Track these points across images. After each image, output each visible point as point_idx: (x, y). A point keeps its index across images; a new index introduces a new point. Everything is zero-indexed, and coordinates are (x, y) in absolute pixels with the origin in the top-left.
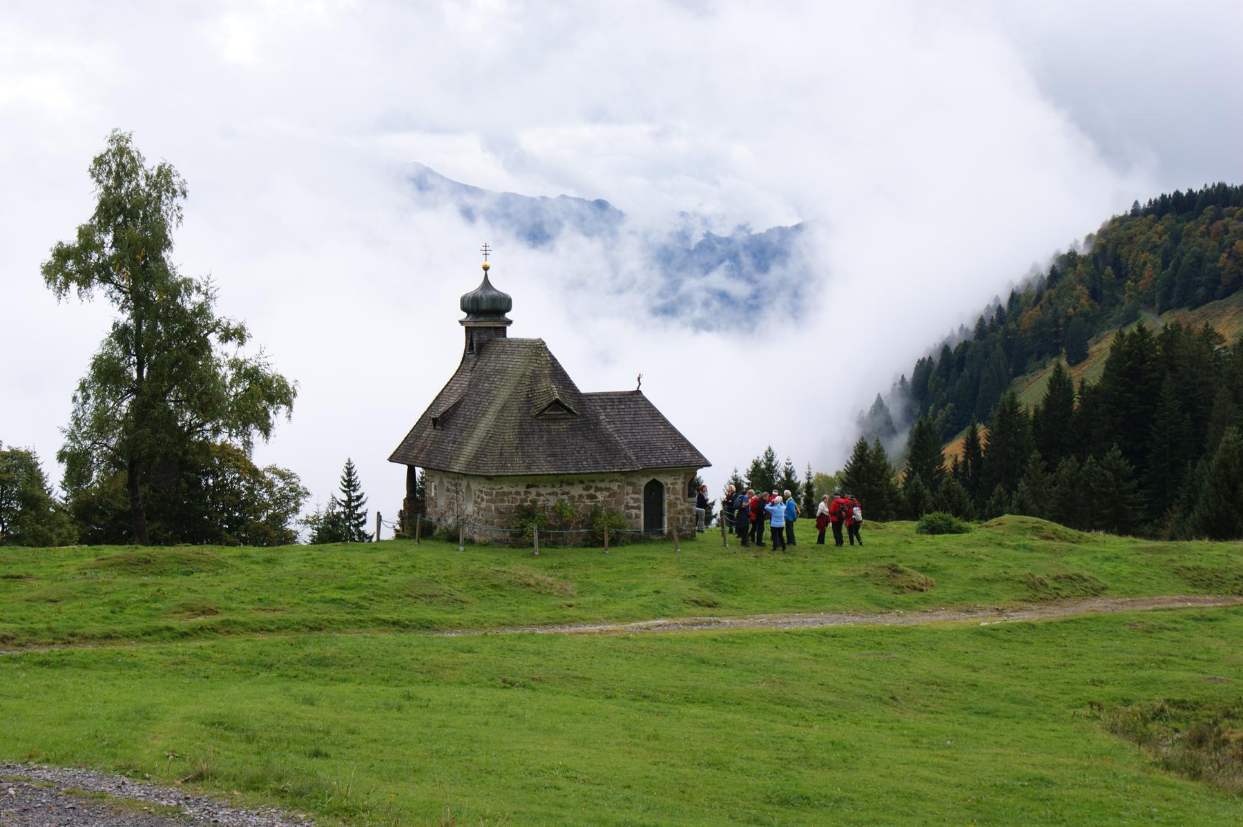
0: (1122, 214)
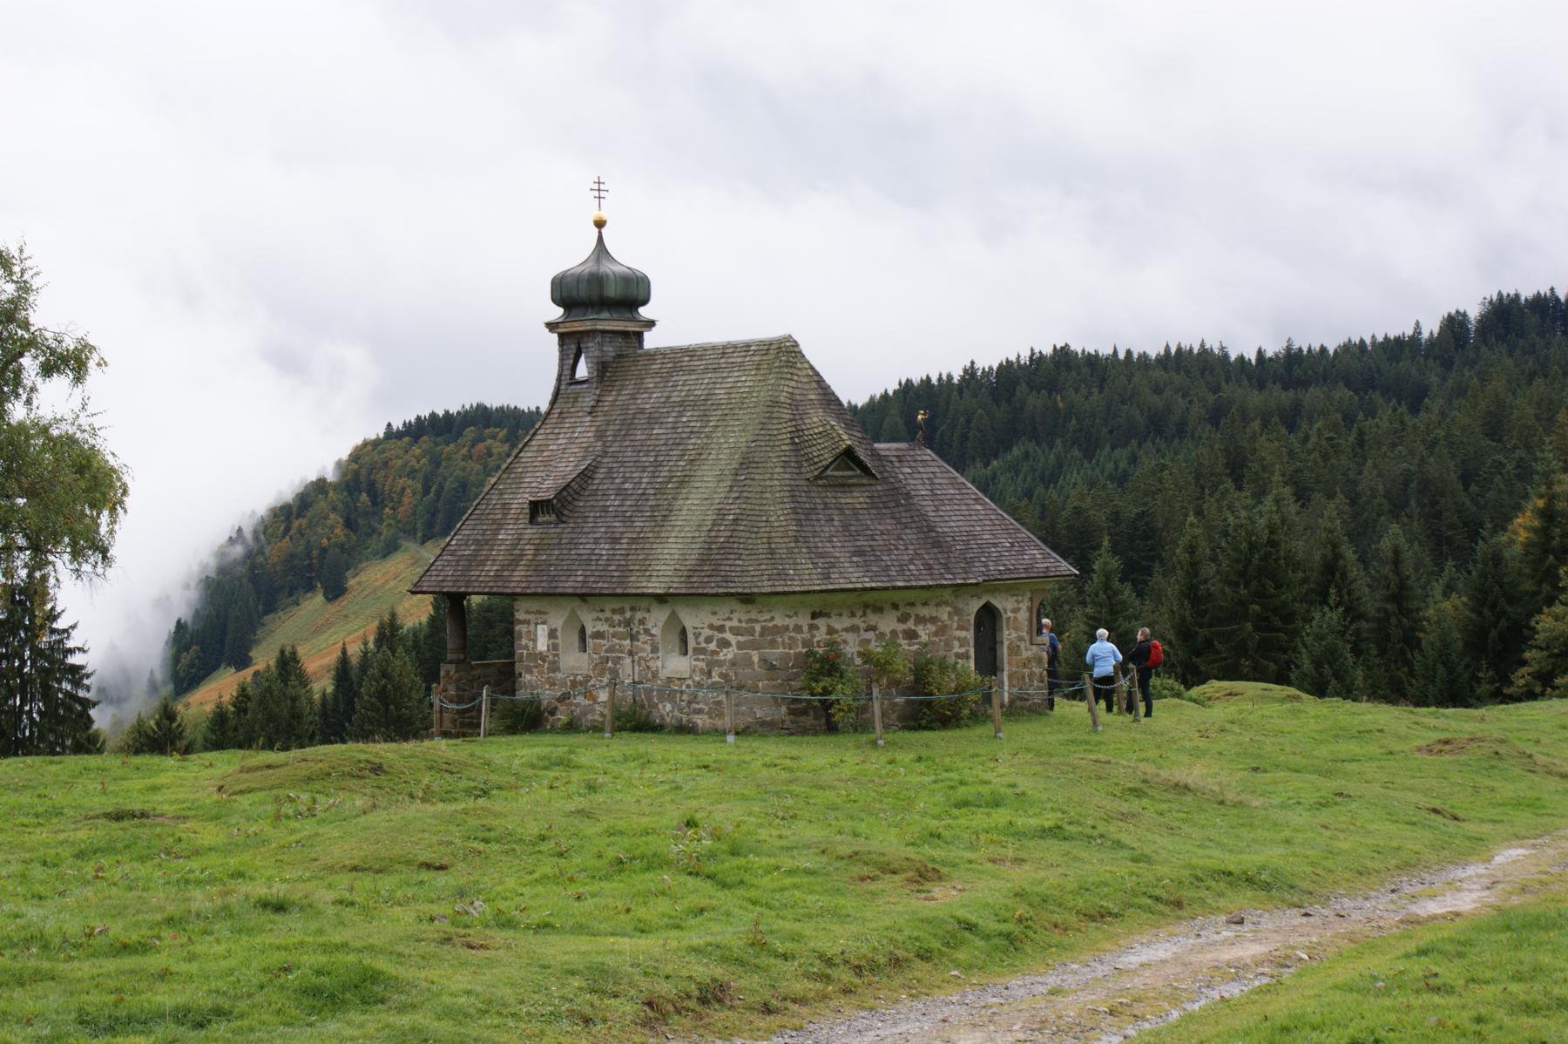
0: (373, 437)
